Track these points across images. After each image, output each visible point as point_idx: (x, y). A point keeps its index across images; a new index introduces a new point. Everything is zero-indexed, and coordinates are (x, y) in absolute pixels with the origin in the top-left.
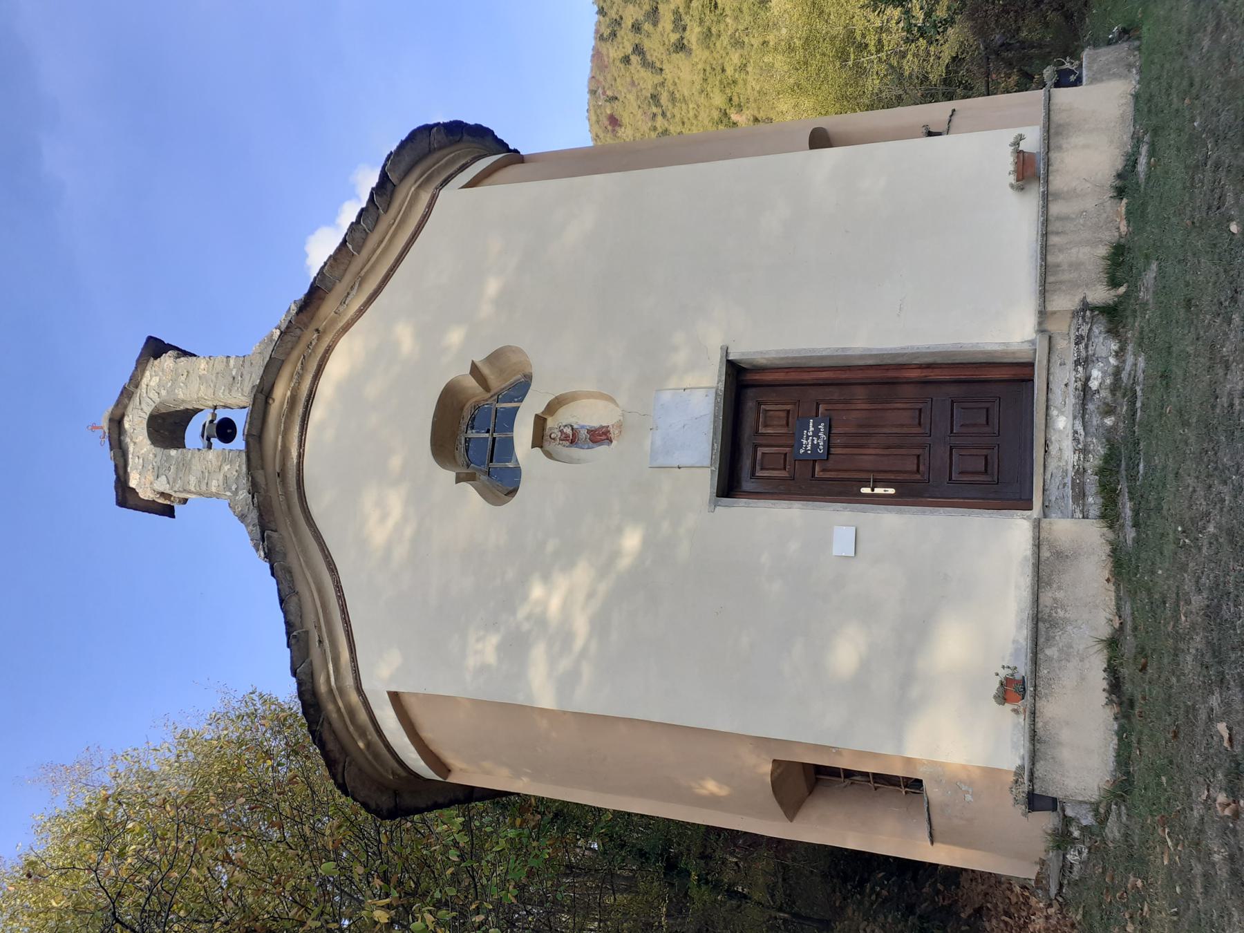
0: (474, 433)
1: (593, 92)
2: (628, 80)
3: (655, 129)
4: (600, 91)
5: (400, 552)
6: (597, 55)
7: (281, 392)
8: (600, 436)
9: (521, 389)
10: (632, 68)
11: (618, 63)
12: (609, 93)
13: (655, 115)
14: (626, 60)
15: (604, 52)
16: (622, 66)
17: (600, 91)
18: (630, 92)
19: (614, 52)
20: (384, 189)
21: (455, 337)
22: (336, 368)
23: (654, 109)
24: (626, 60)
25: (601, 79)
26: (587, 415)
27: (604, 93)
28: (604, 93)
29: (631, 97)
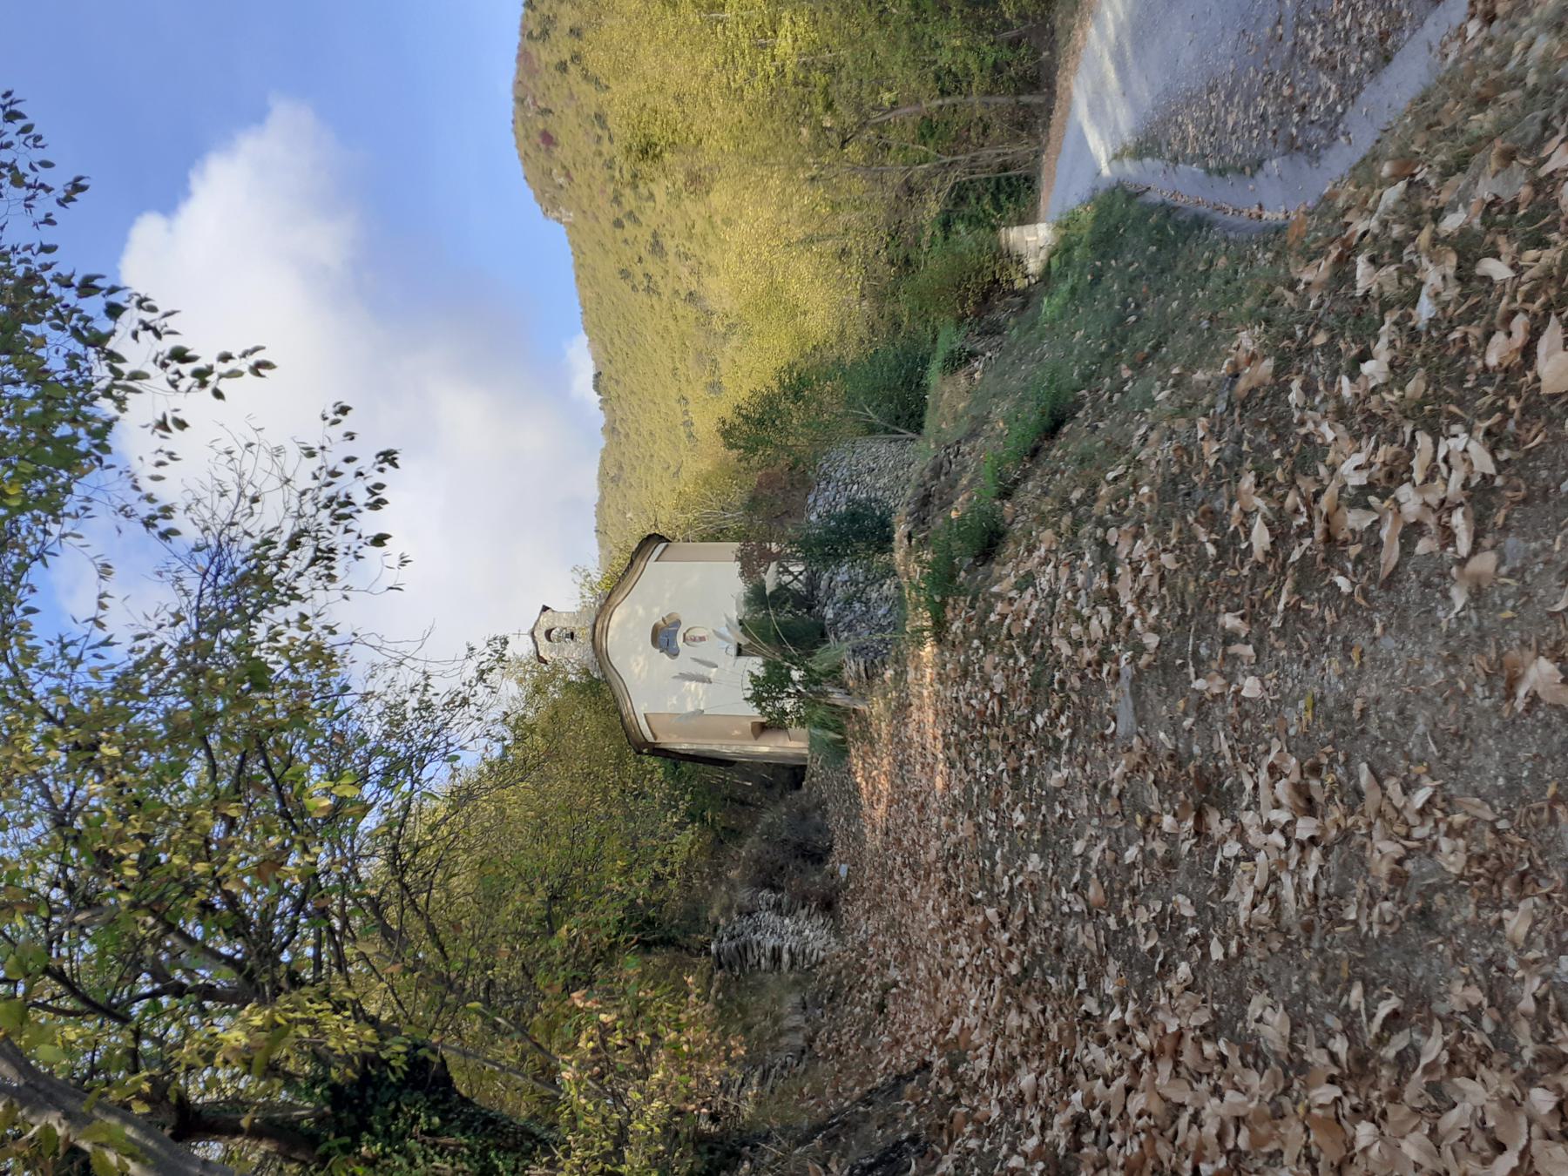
0: (664, 637)
1: (520, 100)
2: (566, 91)
3: (600, 154)
4: (529, 100)
5: (644, 675)
6: (524, 56)
7: (599, 626)
8: (702, 639)
9: (678, 623)
10: (570, 78)
11: (552, 70)
12: (542, 104)
13: (599, 138)
14: (562, 67)
15: (534, 53)
16: (558, 74)
17: (529, 100)
18: (568, 106)
19: (546, 56)
20: (632, 562)
21: (656, 610)
22: (616, 618)
23: (599, 132)
24: (562, 67)
25: (531, 85)
26: (698, 633)
27: (534, 103)
28: (534, 103)
29: (570, 112)
